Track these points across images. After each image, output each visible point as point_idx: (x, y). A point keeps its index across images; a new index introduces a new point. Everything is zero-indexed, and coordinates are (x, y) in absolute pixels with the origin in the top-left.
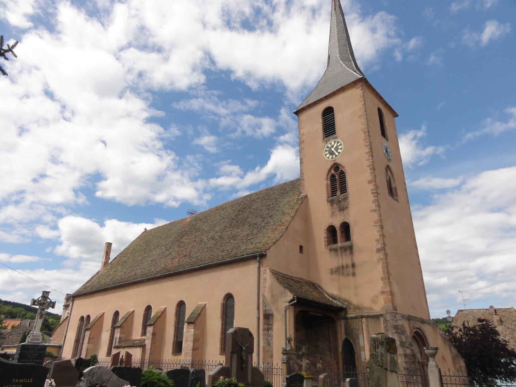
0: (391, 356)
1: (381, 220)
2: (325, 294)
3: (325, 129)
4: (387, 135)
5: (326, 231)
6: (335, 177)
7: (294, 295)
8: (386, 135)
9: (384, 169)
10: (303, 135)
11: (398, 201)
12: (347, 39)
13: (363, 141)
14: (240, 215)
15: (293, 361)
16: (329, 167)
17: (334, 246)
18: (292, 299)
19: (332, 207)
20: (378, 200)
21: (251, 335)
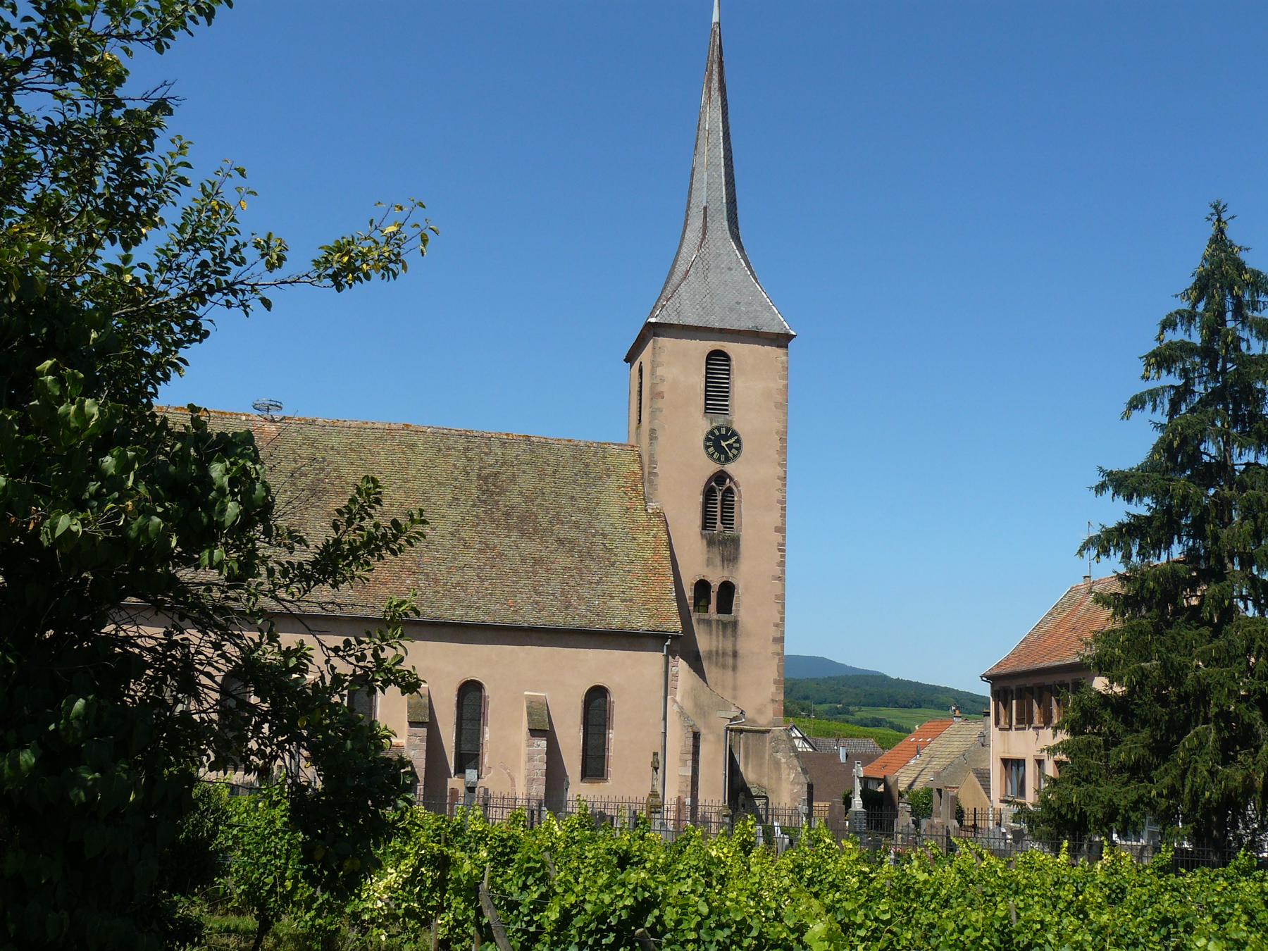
10: (662, 380)
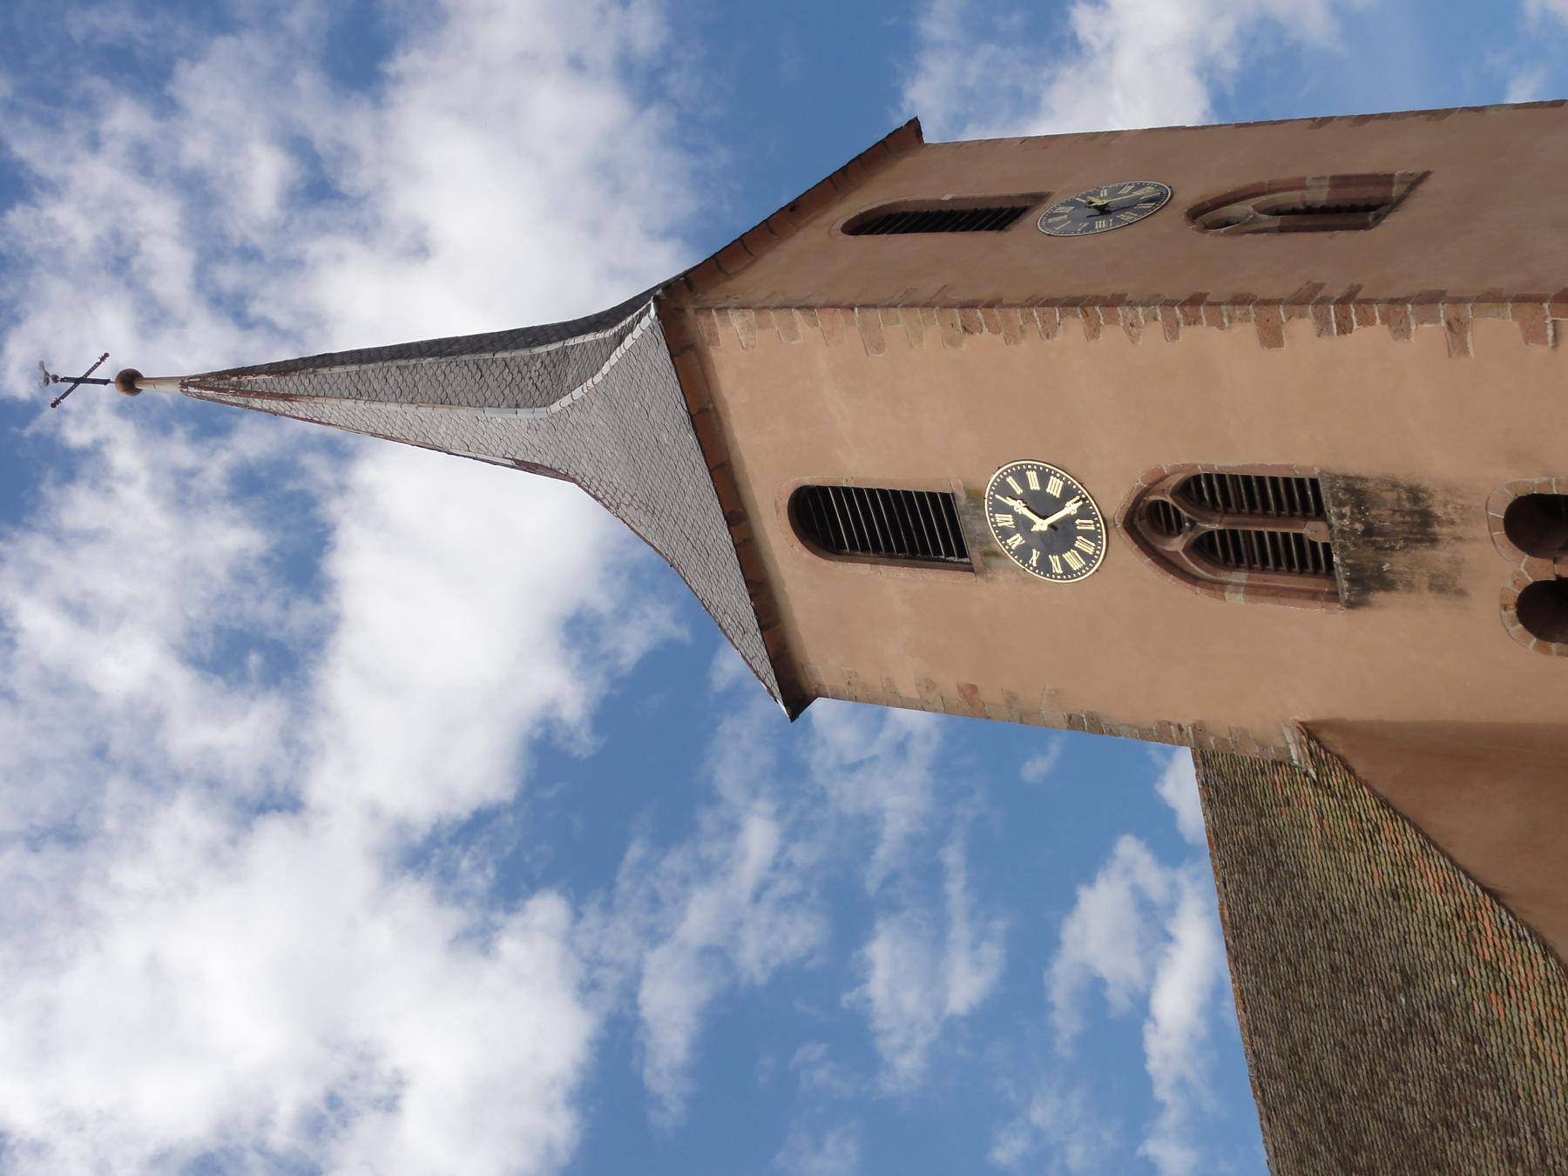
1: (1520, 299)
3: (889, 548)
4: (1010, 198)
5: (1554, 646)
6: (1210, 534)
8: (1007, 205)
9: (1210, 239)
10: (929, 685)
12: (450, 354)
19: (1400, 586)
20: (1393, 301)
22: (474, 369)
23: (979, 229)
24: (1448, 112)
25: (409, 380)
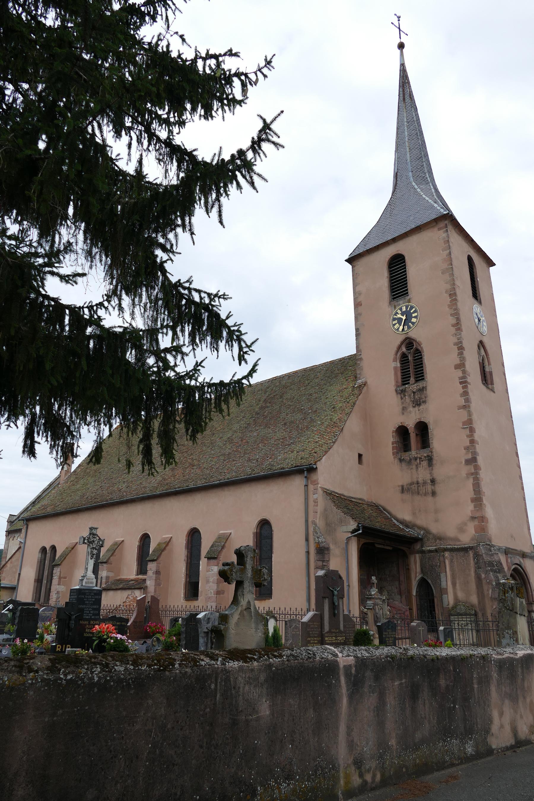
0: (520, 601)
2: (393, 519)
6: (407, 357)
7: (359, 524)
8: (478, 295)
10: (360, 294)
11: (494, 392)
13: (448, 307)
14: (268, 407)
15: (379, 606)
16: (398, 342)
17: (406, 456)
18: (355, 528)
21: (340, 577)
22: (420, 157)
23: (472, 290)
24: (508, 393)
25: (414, 137)
